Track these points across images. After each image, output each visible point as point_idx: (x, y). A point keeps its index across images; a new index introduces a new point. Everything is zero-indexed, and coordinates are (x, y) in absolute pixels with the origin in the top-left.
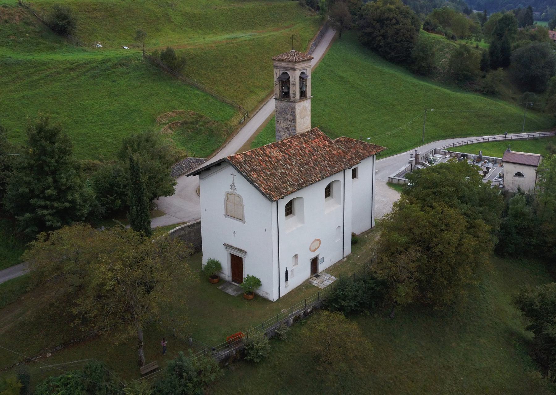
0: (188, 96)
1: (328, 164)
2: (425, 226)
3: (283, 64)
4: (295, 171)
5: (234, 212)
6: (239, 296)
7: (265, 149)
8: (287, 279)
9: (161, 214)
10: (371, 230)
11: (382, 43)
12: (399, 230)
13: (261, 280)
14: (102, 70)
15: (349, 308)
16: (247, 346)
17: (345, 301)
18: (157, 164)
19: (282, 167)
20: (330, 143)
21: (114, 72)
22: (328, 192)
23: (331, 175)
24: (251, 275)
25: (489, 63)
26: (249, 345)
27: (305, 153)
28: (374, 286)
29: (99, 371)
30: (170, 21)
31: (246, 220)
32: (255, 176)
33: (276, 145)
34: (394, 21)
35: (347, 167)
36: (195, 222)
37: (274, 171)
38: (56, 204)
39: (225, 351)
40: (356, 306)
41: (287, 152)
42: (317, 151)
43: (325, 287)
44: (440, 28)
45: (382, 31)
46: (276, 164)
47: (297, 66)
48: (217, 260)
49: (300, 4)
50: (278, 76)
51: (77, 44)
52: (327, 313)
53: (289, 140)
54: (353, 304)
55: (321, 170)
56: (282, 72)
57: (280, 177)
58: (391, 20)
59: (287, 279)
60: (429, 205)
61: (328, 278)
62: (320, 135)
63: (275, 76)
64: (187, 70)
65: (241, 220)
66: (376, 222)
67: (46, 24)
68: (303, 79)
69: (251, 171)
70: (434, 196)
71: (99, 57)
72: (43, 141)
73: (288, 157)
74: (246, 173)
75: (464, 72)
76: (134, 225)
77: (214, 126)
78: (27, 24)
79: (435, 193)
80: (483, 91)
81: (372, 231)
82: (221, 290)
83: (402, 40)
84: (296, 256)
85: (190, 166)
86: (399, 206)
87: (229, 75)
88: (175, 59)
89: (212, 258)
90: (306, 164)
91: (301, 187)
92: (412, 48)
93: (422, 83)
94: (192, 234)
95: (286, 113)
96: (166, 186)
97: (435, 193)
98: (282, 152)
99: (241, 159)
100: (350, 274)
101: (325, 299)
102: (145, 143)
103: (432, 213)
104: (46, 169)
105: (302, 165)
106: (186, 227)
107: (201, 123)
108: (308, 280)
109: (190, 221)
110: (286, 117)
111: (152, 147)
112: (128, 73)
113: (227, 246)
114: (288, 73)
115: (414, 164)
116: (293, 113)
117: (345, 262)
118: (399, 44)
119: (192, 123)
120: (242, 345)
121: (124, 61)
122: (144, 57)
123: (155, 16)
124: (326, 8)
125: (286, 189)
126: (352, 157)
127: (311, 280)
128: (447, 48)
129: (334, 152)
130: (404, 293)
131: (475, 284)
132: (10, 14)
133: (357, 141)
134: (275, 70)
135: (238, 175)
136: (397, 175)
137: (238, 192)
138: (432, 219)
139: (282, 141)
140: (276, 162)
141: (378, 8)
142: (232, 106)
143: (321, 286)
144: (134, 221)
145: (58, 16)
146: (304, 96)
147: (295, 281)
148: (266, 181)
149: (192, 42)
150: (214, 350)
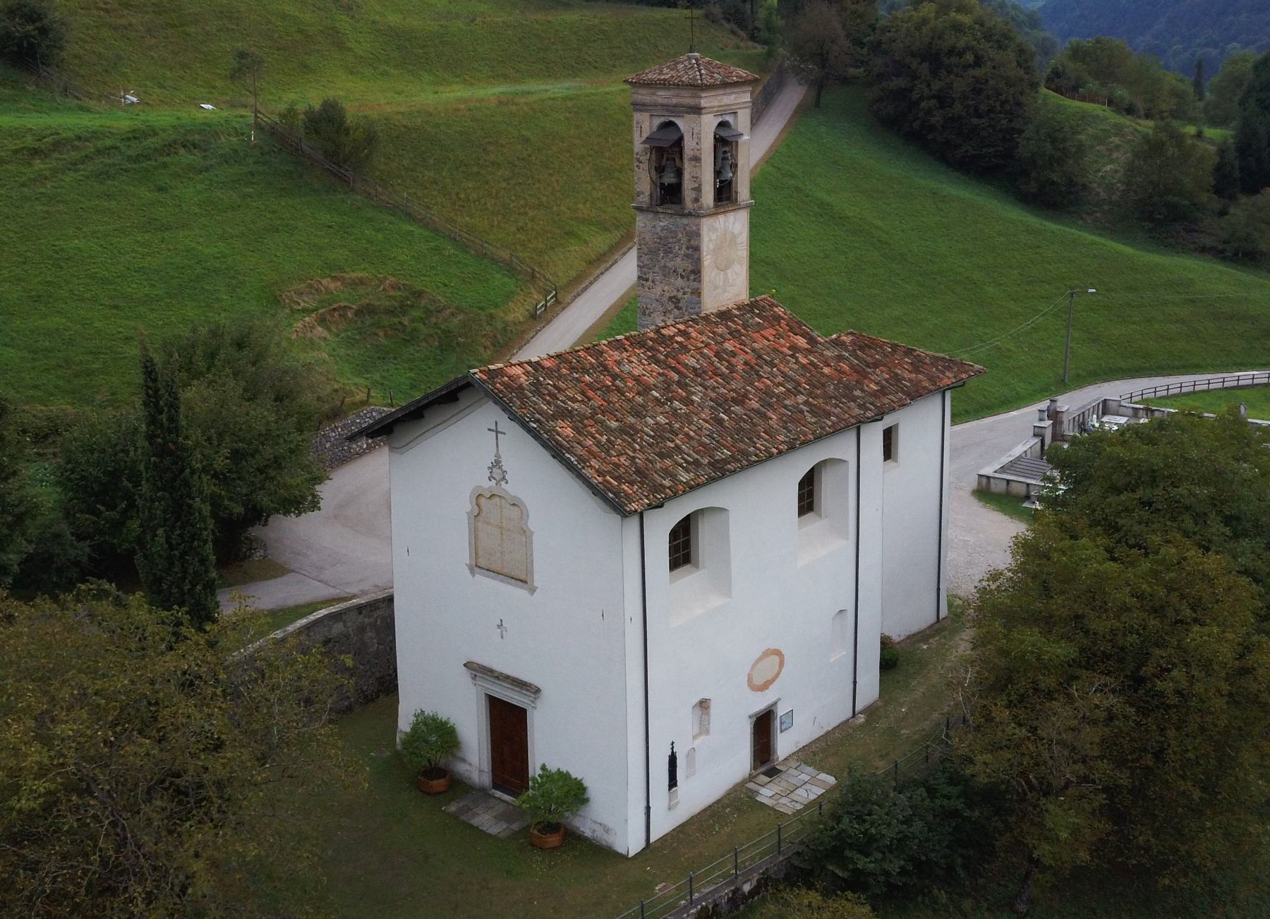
0: (380, 236)
1: (806, 403)
2: (1125, 609)
3: (662, 96)
4: (702, 420)
5: (501, 554)
6: (515, 836)
7: (602, 353)
8: (673, 782)
9: (274, 570)
10: (938, 629)
11: (937, 119)
12: (1046, 622)
13: (586, 783)
14: (129, 159)
15: (882, 879)
17: (867, 856)
18: (263, 414)
19: (659, 409)
20: (812, 341)
21: (165, 165)
22: (808, 499)
23: (818, 438)
24: (553, 767)
25: (1237, 174)
27: (731, 368)
28: (959, 804)
30: (341, 46)
31: (538, 579)
32: (569, 431)
33: (639, 342)
34: (969, 57)
35: (869, 414)
36: (380, 596)
37: (631, 420)
40: (903, 872)
41: (673, 363)
43: (799, 807)
44: (1093, 85)
45: (937, 85)
46: (639, 399)
47: (707, 100)
48: (443, 715)
49: (707, 16)
50: (645, 135)
51: (65, 92)
52: (814, 897)
53: (682, 327)
54: (894, 866)
56: (657, 122)
57: (655, 450)
58: (961, 54)
59: (673, 782)
60: (1132, 541)
61: (805, 777)
62: (778, 318)
64: (382, 167)
65: (523, 581)
66: (950, 605)
69: (554, 417)
70: (1145, 514)
71: (122, 123)
73: (676, 377)
74: (537, 421)
75: (1171, 198)
76: (160, 592)
77: (455, 321)
80: (1222, 251)
82: (454, 816)
83: (991, 110)
84: (703, 705)
86: (1025, 548)
87: (504, 185)
90: (735, 401)
91: (720, 472)
92: (1020, 132)
93: (1051, 226)
94: (370, 634)
95: (668, 251)
96: (289, 481)
98: (657, 362)
99: (523, 379)
100: (882, 766)
102: (232, 354)
103: (1145, 566)
105: (722, 403)
106: (349, 609)
107: (415, 314)
108: (740, 786)
109: (364, 593)
111: (254, 364)
112: (207, 169)
113: (477, 670)
114: (680, 123)
115: (1048, 440)
116: (694, 252)
117: (861, 726)
118: (984, 122)
119: (390, 312)
122: (258, 127)
123: (301, 31)
124: (779, 22)
125: (673, 477)
126: (883, 387)
127: (751, 785)
128: (1116, 135)
129: (826, 370)
130: (1067, 828)
134: (637, 116)
135: (513, 431)
136: (1003, 469)
137: (511, 488)
138: (1150, 584)
139: (658, 331)
140: (639, 394)
141: (925, 21)
142: (510, 269)
143: (787, 806)
144: (158, 581)
147: (703, 787)
148: (607, 448)
149: (400, 99)
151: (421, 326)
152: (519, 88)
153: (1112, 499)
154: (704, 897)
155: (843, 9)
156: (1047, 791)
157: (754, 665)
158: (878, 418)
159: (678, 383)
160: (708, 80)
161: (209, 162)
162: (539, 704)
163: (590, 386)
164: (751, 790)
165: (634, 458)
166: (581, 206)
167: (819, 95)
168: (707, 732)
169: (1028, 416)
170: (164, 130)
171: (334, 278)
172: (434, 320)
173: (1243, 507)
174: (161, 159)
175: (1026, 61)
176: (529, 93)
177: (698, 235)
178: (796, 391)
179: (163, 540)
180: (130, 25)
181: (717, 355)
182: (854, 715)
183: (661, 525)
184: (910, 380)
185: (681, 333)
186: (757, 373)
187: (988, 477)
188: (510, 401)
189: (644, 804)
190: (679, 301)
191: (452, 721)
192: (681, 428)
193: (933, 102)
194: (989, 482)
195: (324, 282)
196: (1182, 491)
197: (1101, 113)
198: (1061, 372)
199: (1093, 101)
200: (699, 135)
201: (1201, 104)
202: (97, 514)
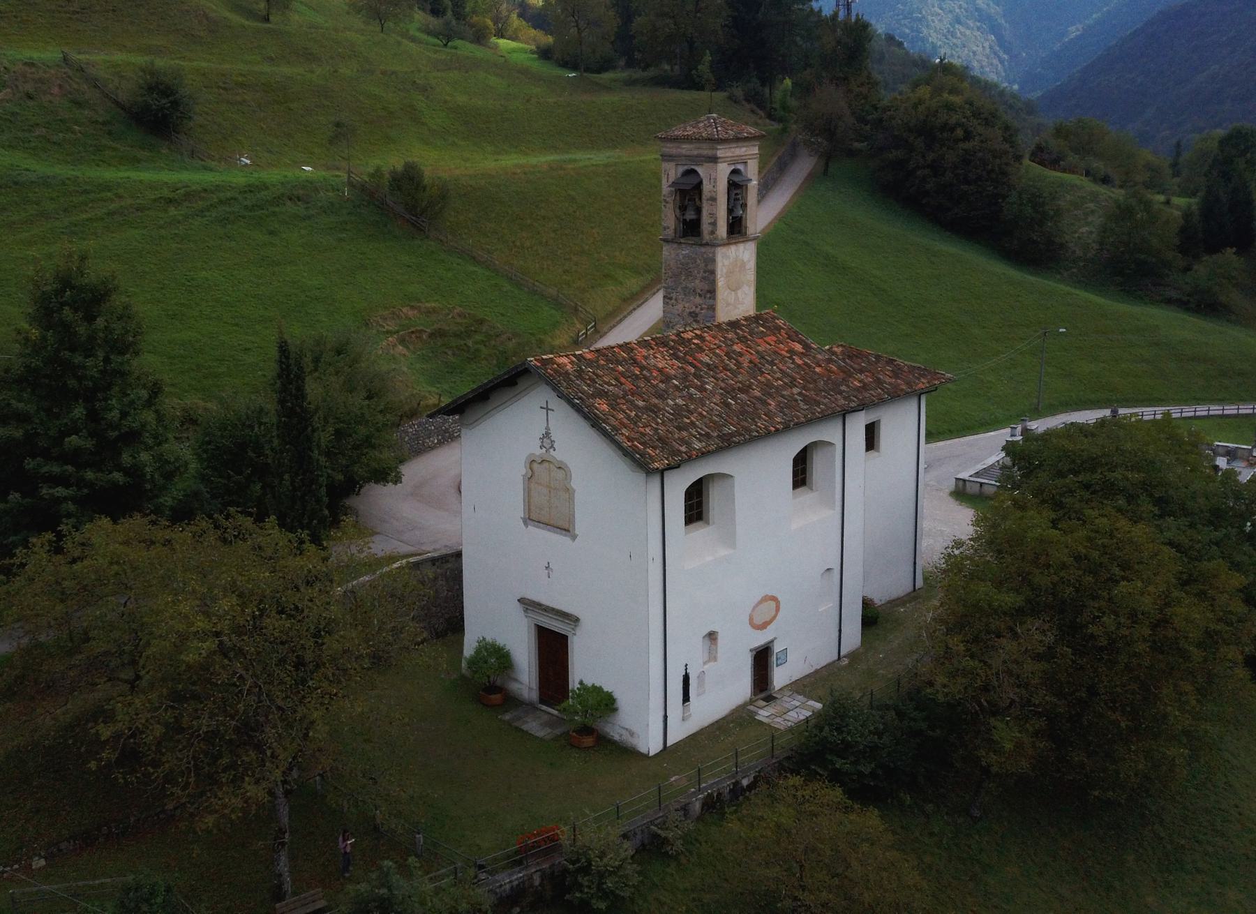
0: (450, 275)
1: (800, 394)
2: (1064, 566)
3: (686, 149)
4: (714, 404)
5: (549, 510)
7: (632, 349)
8: (686, 698)
10: (914, 596)
13: (616, 695)
14: (246, 207)
16: (573, 863)
20: (807, 347)
22: (801, 474)
24: (589, 682)
26: (578, 860)
27: (739, 364)
28: (924, 726)
29: (159, 900)
34: (959, 132)
35: (853, 405)
38: (90, 475)
39: (511, 875)
41: (690, 359)
42: (772, 363)
44: (1072, 158)
45: (931, 156)
46: (662, 386)
49: (730, 98)
50: (671, 180)
51: (192, 154)
55: (781, 408)
56: (681, 169)
57: (678, 429)
58: (953, 129)
59: (686, 698)
61: (798, 704)
62: (779, 328)
63: (664, 181)
65: (566, 530)
66: (925, 579)
67: (123, 108)
68: (736, 186)
69: (593, 396)
70: (1087, 495)
71: (239, 179)
72: (67, 311)
73: (693, 370)
74: (580, 398)
78: (78, 104)
79: (1087, 487)
81: (915, 598)
84: (712, 636)
85: (446, 431)
87: (553, 235)
88: (424, 188)
89: (489, 639)
91: (727, 444)
92: (1004, 197)
93: (1032, 278)
95: (689, 275)
97: (1087, 487)
98: (677, 358)
99: (569, 367)
101: (790, 753)
103: (1082, 533)
104: (72, 383)
105: (730, 391)
108: (743, 707)
110: (691, 285)
112: (309, 218)
113: (529, 605)
114: (700, 170)
116: (710, 275)
119: (457, 335)
120: (560, 860)
121: (301, 192)
122: (351, 184)
124: (793, 103)
125: (688, 444)
126: (865, 384)
127: (751, 708)
128: (1092, 201)
129: (818, 370)
131: (1206, 732)
132: (41, 81)
133: (878, 357)
134: (666, 165)
136: (977, 474)
137: (558, 455)
140: (662, 381)
141: (921, 101)
143: (781, 723)
145: (151, 89)
146: (739, 232)
150: (481, 867)
151: (482, 347)
152: (567, 157)
153: (1059, 482)
154: (711, 786)
155: (850, 91)
156: (995, 711)
157: (757, 605)
158: (862, 407)
159: (695, 375)
160: (723, 136)
161: (311, 212)
162: (578, 632)
163: (622, 374)
164: (752, 712)
165: (656, 429)
166: (617, 254)
167: (827, 165)
168: (715, 659)
169: (1002, 435)
170: (274, 186)
171: (412, 308)
172: (493, 343)
173: (1171, 492)
174: (272, 209)
175: (1011, 135)
176: (575, 160)
177: (713, 261)
178: (793, 384)
179: (288, 483)
180: (244, 101)
181: (727, 354)
182: (839, 658)
183: (678, 484)
184: (890, 384)
185: (697, 336)
186: (760, 369)
187: (964, 481)
188: (560, 384)
189: (662, 713)
190: (697, 315)
191: (507, 648)
192: (695, 409)
193: (927, 171)
194: (964, 485)
195: (404, 310)
196: (1117, 475)
197: (1078, 182)
198: (1035, 401)
199: (1073, 173)
200: (716, 179)
201: (1177, 180)
202: (229, 477)
